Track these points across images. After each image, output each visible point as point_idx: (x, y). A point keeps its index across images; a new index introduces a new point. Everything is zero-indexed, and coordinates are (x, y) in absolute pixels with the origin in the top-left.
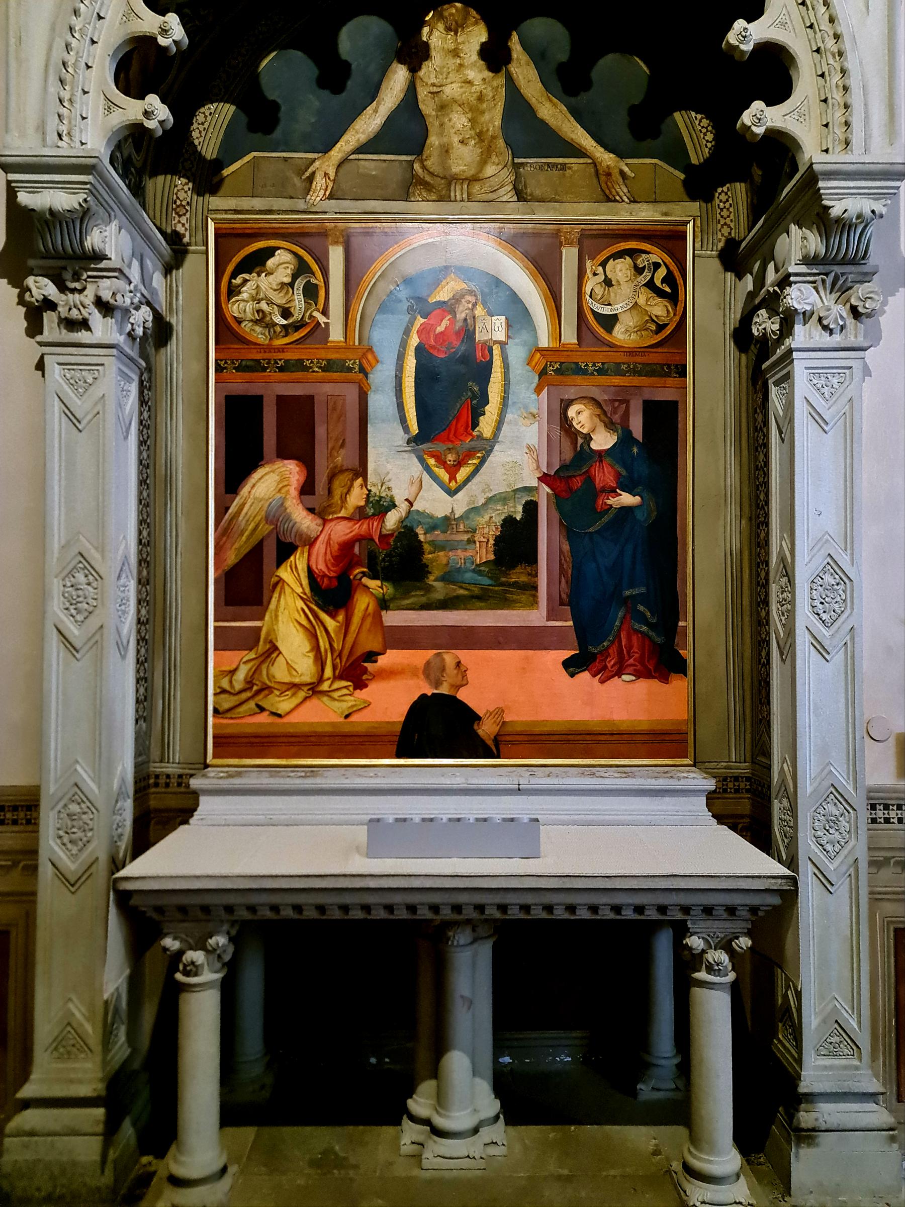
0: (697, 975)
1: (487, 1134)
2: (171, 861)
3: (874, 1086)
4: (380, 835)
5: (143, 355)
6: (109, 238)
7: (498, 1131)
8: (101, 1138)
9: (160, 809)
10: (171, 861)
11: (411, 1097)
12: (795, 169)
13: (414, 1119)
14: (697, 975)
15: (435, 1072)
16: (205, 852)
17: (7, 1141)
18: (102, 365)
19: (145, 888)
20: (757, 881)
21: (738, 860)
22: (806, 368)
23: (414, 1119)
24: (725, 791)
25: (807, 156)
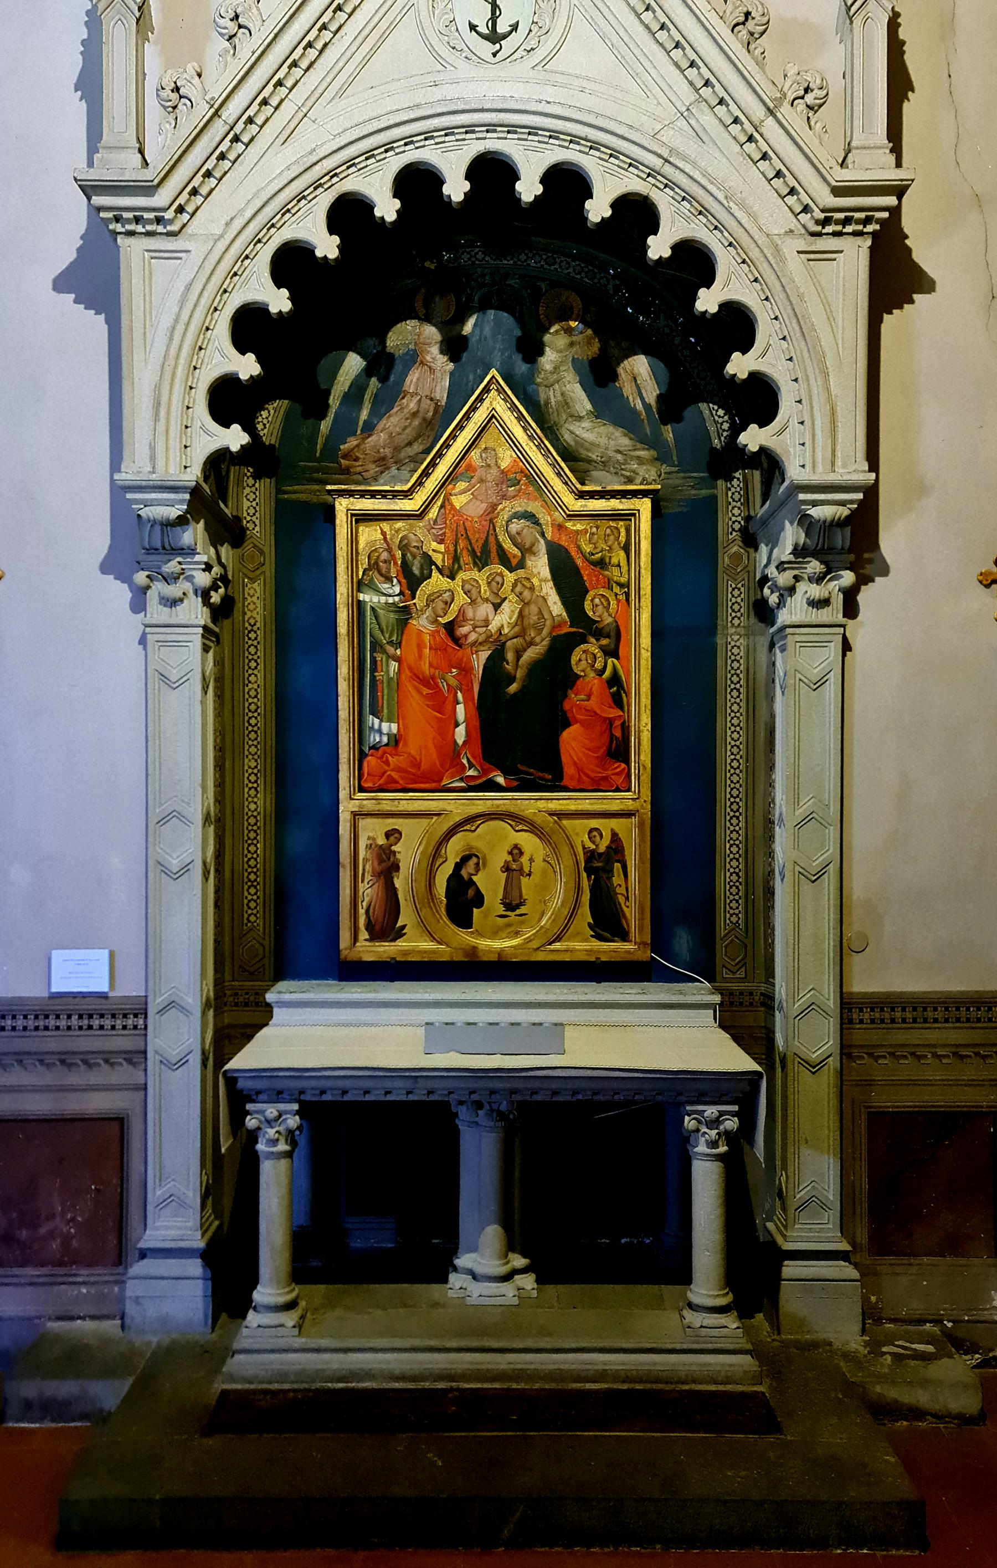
3: (844, 1246)
4: (436, 1035)
9: (236, 1013)
14: (696, 1150)
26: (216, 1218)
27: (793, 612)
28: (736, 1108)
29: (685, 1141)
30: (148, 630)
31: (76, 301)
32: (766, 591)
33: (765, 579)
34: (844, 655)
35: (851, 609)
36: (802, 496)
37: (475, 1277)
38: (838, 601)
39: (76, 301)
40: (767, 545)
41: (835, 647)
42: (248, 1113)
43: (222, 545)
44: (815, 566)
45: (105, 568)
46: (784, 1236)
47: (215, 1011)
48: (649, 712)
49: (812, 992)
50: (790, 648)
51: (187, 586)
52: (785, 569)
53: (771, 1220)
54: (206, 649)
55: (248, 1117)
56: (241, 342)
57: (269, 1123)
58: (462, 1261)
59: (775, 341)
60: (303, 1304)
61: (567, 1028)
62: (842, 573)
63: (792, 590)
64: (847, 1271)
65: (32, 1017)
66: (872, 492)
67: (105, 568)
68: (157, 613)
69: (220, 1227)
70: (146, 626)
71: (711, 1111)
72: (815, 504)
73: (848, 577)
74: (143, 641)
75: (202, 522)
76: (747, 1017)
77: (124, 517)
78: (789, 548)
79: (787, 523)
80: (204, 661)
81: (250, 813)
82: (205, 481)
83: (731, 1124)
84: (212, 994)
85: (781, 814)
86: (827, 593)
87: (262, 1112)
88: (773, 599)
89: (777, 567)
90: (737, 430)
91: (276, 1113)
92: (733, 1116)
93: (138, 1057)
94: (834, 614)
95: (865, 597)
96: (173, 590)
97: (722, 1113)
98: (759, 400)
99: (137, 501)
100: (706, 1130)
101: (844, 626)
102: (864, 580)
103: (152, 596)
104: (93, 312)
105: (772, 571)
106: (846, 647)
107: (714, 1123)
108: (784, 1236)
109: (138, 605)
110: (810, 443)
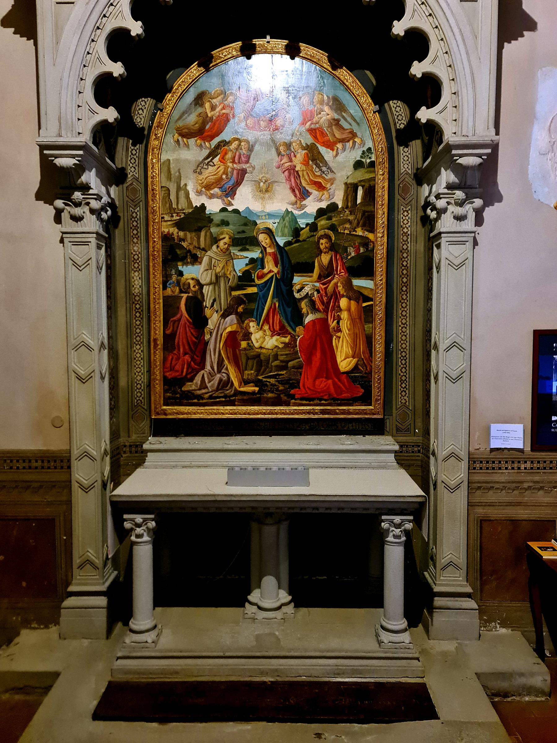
0: (387, 539)
1: (284, 609)
2: (135, 486)
3: (469, 590)
4: (235, 474)
5: (107, 230)
6: (90, 177)
7: (290, 609)
8: (105, 609)
9: (124, 459)
10: (135, 486)
11: (249, 595)
12: (441, 142)
13: (250, 603)
14: (387, 539)
15: (259, 586)
16: (149, 481)
17: (62, 610)
18: (90, 242)
19: (258, 499)
20: (322, 497)
21: (405, 487)
22: (447, 242)
23: (250, 603)
24: (401, 452)
25: (446, 138)
26: (115, 570)
27: (446, 224)
28: (411, 518)
29: (382, 535)
30: (64, 235)
31: (15, 33)
32: (429, 211)
33: (427, 204)
34: (474, 248)
35: (479, 221)
36: (454, 152)
37: (260, 608)
38: (472, 216)
39: (15, 33)
40: (428, 186)
41: (469, 245)
42: (126, 520)
43: (111, 187)
44: (460, 194)
45: (39, 196)
46: (435, 584)
47: (111, 458)
48: (162, 439)
49: (452, 447)
50: (443, 245)
51: (86, 209)
52: (441, 198)
53: (427, 571)
54: (99, 247)
55: (125, 523)
56: (113, 56)
57: (139, 526)
58: (254, 596)
59: (440, 54)
60: (159, 626)
61: (310, 470)
62: (474, 200)
63: (445, 210)
64: (472, 604)
65: (9, 461)
66: (495, 147)
67: (39, 196)
68: (68, 225)
69: (117, 578)
70: (63, 233)
71: (397, 519)
72: (461, 156)
73: (478, 202)
74: (62, 241)
75: (94, 170)
76: (416, 460)
77: (47, 166)
78: (444, 185)
79: (442, 169)
80: (97, 254)
81: (406, 301)
82: (94, 143)
83: (409, 526)
84: (108, 447)
85: (435, 343)
86: (465, 212)
87: (133, 520)
88: (433, 215)
89: (435, 197)
90: (414, 110)
91: (141, 520)
92: (410, 522)
93: (68, 485)
94: (469, 225)
95: (488, 213)
96: (78, 211)
97: (403, 521)
98: (429, 90)
99: (52, 156)
100: (395, 529)
101: (474, 232)
102: (488, 203)
103: (65, 216)
104: (25, 38)
105: (432, 199)
106: (475, 243)
107: (398, 526)
108: (435, 584)
109: (58, 219)
110: (460, 116)
